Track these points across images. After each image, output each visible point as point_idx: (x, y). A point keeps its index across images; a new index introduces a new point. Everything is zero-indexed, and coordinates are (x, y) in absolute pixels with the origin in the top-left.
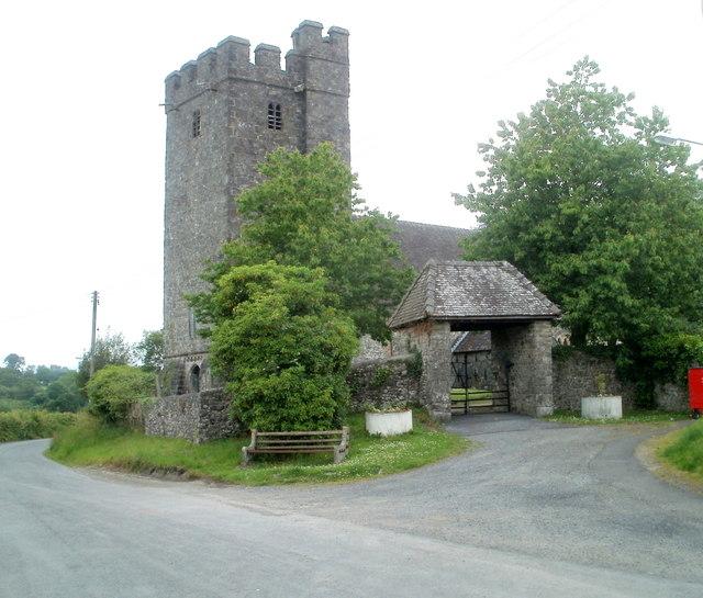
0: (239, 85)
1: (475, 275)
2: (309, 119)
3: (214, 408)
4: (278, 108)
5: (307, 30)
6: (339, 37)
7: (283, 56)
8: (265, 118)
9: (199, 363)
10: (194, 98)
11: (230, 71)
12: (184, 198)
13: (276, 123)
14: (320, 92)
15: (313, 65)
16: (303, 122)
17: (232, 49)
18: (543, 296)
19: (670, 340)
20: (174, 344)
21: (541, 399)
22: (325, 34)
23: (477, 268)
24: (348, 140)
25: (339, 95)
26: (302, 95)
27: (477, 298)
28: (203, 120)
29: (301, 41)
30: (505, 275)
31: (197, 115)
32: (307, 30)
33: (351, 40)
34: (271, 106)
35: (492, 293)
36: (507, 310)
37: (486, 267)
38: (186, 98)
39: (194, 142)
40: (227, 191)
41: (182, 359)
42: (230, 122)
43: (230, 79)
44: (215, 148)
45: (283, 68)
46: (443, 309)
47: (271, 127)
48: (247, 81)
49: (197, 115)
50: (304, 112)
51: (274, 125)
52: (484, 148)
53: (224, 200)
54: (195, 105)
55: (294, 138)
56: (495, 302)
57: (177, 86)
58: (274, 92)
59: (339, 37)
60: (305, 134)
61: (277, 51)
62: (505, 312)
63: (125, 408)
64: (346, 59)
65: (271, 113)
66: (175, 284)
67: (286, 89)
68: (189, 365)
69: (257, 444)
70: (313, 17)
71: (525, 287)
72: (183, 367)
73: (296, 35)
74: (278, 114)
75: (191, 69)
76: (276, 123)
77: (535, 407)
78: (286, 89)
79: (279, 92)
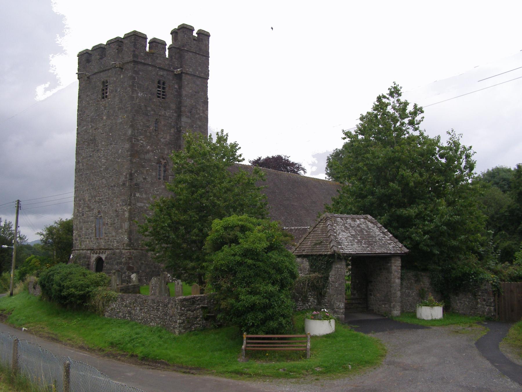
0: (140, 67)
1: (353, 224)
2: (184, 93)
3: (189, 310)
4: (164, 84)
5: (182, 32)
6: (204, 36)
7: (167, 47)
8: (155, 90)
9: (103, 257)
10: (104, 71)
11: (135, 56)
12: (93, 141)
13: (161, 95)
14: (191, 75)
15: (188, 56)
16: (179, 95)
17: (136, 38)
18: (396, 240)
19: (481, 276)
20: (81, 242)
21: (394, 306)
22: (195, 34)
23: (353, 220)
24: (207, 110)
25: (203, 77)
26: (179, 77)
27: (359, 241)
28: (110, 88)
29: (179, 38)
30: (370, 225)
31: (105, 84)
32: (182, 32)
33: (211, 39)
34: (159, 82)
35: (369, 239)
36: (378, 250)
37: (358, 219)
38: (96, 71)
39: (103, 102)
40: (130, 139)
41: (89, 252)
42: (133, 92)
43: (134, 62)
44: (120, 109)
45: (167, 56)
46: (342, 248)
47: (159, 97)
48: (145, 64)
49: (105, 84)
50: (180, 87)
51: (161, 96)
52: (348, 134)
53: (127, 146)
54: (103, 76)
55: (173, 106)
56: (370, 244)
57: (88, 61)
58: (161, 73)
59: (204, 36)
60: (180, 102)
61: (164, 44)
62: (378, 251)
63: (85, 298)
64: (208, 53)
65: (159, 87)
66: (84, 200)
67: (169, 71)
68: (94, 257)
69: (246, 347)
70: (188, 22)
71: (384, 233)
72: (90, 258)
73: (174, 33)
74: (164, 88)
75: (99, 49)
76: (161, 95)
77: (391, 311)
78: (169, 71)
79: (165, 73)
